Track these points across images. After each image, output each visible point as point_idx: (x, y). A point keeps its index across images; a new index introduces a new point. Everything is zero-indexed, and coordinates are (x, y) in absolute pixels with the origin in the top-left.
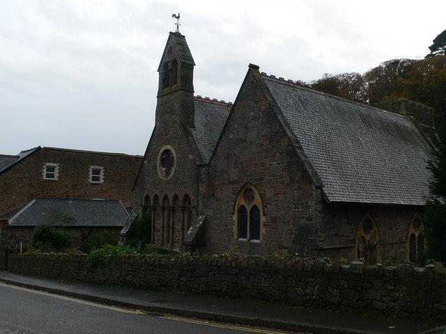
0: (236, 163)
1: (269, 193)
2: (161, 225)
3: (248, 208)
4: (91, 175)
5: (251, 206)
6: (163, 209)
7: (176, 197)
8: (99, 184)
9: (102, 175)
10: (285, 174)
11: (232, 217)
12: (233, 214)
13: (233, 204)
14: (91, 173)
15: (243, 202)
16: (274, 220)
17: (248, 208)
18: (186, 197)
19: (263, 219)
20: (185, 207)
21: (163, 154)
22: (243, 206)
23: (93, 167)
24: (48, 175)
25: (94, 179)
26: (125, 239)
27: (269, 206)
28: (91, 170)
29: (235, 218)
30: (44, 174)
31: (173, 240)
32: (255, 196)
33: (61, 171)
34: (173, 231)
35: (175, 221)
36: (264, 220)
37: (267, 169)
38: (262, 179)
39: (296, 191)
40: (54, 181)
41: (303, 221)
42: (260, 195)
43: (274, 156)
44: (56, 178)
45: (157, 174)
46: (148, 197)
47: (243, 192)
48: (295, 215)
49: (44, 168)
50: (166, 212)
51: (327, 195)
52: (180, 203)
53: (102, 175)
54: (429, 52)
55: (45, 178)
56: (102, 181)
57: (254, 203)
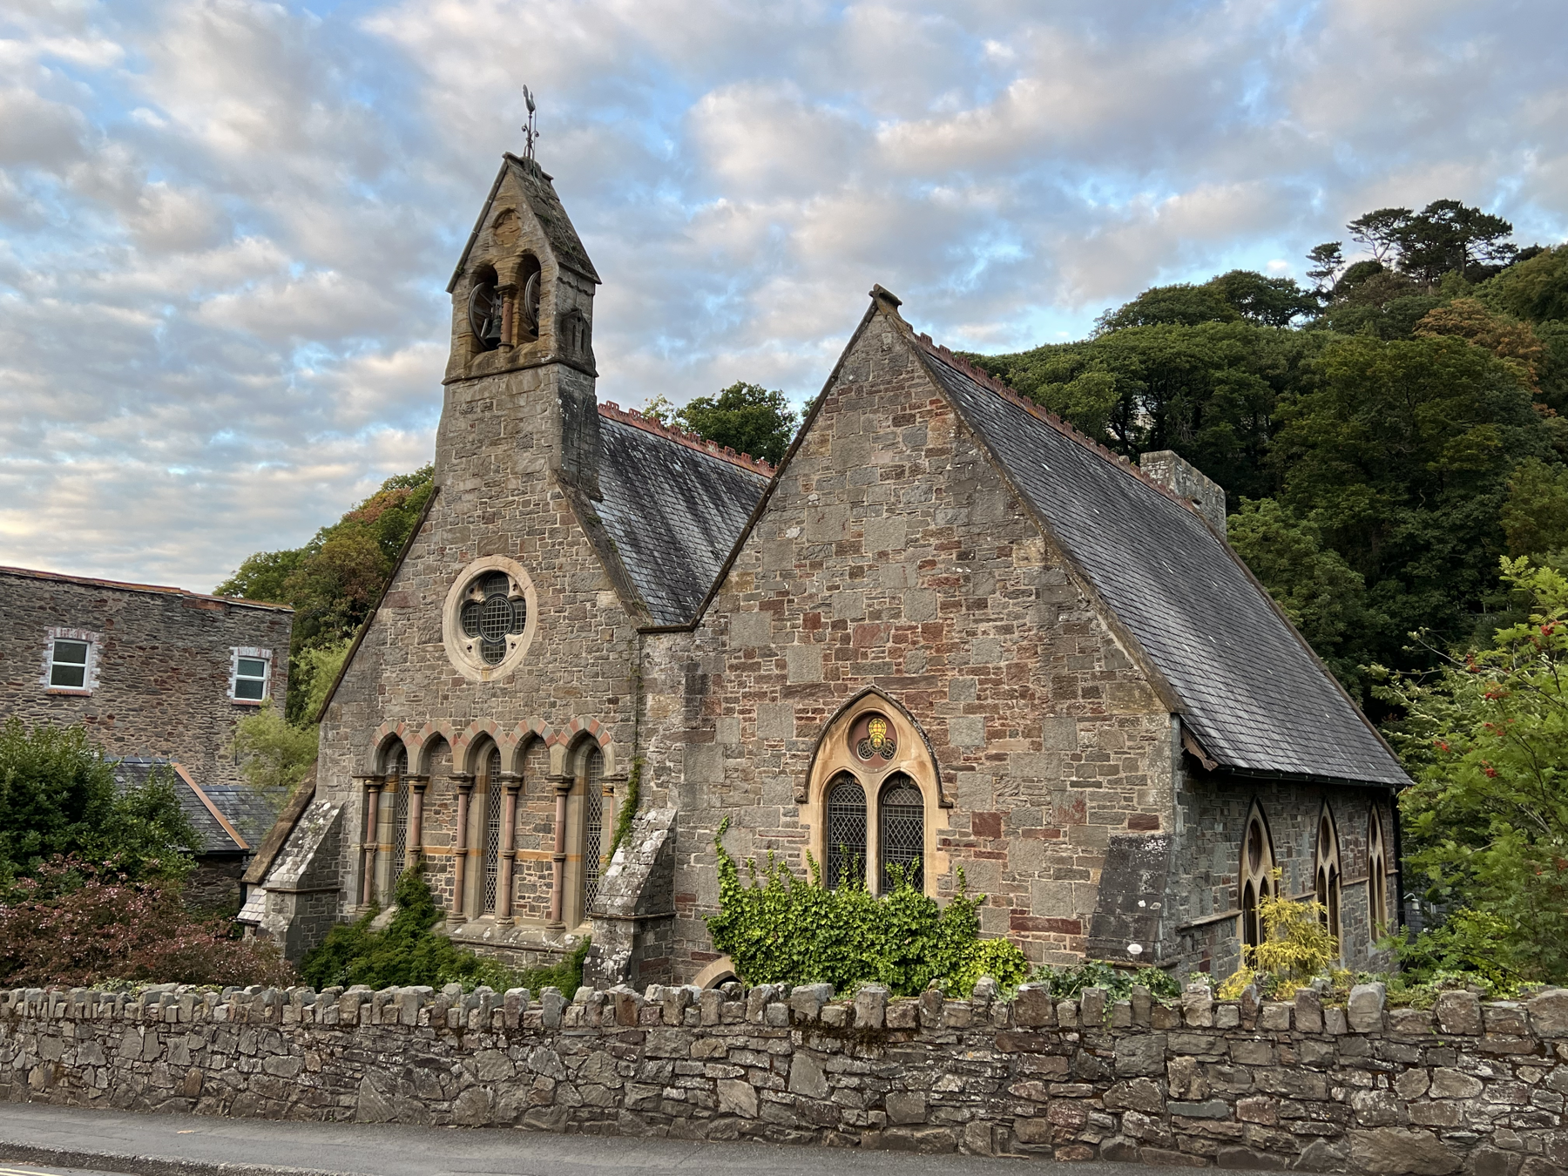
0: (813, 622)
1: (964, 732)
2: (457, 847)
3: (870, 783)
4: (50, 661)
5: (881, 778)
6: (468, 786)
7: (436, 743)
8: (257, 707)
9: (91, 664)
10: (1032, 663)
11: (795, 813)
12: (803, 800)
13: (801, 765)
14: (49, 654)
15: (838, 756)
16: (988, 825)
17: (870, 783)
18: (584, 743)
19: (935, 823)
20: (572, 781)
21: (470, 588)
22: (846, 775)
25: (60, 676)
26: (291, 903)
28: (235, 659)
31: (510, 899)
34: (513, 870)
35: (524, 829)
36: (944, 825)
37: (953, 647)
46: (392, 744)
47: (845, 724)
48: (1080, 805)
49: (45, 647)
50: (478, 800)
52: (456, 761)
53: (91, 664)
54: (450, 295)
56: (89, 684)
57: (891, 767)
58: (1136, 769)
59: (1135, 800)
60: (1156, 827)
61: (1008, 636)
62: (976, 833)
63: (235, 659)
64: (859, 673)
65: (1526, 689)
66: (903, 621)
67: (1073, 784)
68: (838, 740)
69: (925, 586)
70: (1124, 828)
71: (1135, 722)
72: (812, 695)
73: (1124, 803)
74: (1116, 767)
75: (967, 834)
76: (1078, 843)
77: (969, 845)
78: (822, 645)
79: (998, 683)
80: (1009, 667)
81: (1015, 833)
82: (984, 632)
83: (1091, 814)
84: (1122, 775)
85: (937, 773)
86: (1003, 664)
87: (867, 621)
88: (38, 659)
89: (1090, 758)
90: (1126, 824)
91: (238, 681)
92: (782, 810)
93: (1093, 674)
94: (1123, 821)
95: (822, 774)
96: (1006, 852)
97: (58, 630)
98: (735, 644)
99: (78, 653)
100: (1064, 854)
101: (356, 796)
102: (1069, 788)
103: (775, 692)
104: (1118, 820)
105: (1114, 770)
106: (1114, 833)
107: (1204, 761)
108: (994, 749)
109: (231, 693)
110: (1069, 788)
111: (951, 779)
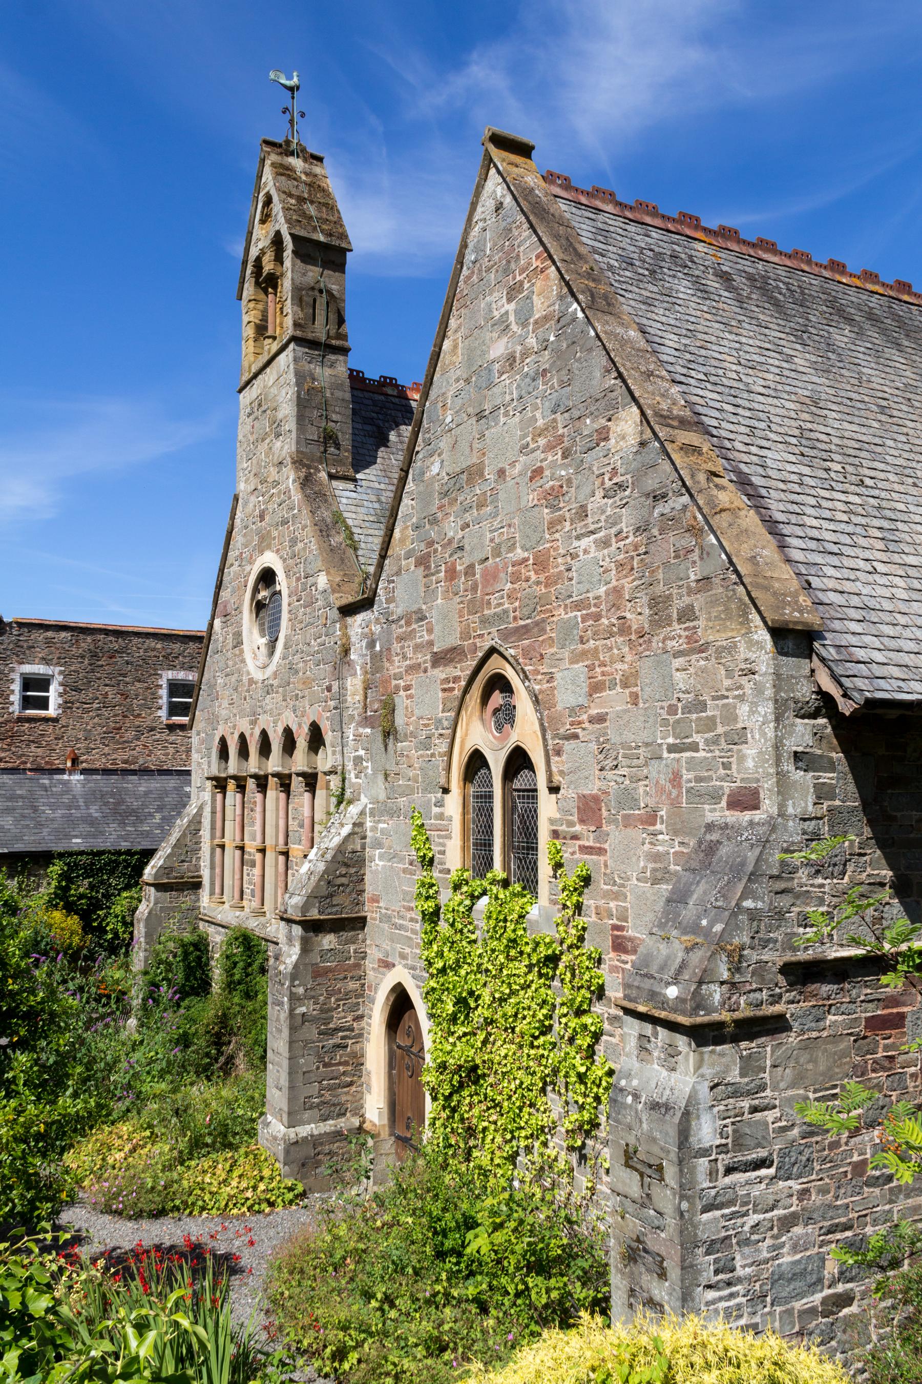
10: (628, 584)
11: (440, 804)
13: (444, 748)
14: (164, 692)
21: (256, 590)
23: (170, 674)
24: (27, 702)
27: (568, 746)
29: (453, 805)
30: (15, 698)
32: (519, 712)
33: (69, 687)
38: (540, 626)
39: (679, 662)
40: (46, 720)
41: (717, 813)
42: (536, 701)
43: (582, 513)
44: (52, 712)
45: (243, 661)
48: (676, 779)
49: (13, 681)
51: (346, 515)
53: (54, 694)
55: (16, 708)
58: (735, 719)
59: (734, 766)
60: (756, 807)
61: (606, 551)
62: (582, 821)
63: (163, 682)
64: (485, 628)
65: (428, 555)
66: (519, 553)
67: (672, 749)
68: (471, 713)
69: (535, 502)
70: (722, 809)
71: (731, 649)
72: (452, 660)
73: (722, 772)
74: (712, 719)
75: (571, 824)
76: (676, 833)
77: (575, 837)
78: (457, 599)
79: (597, 617)
80: (607, 594)
81: (615, 821)
82: (586, 552)
83: (687, 792)
84: (720, 730)
85: (545, 746)
86: (602, 590)
87: (491, 561)
88: (156, 697)
89: (688, 709)
90: (724, 804)
91: (48, 691)
92: (433, 800)
93: (689, 587)
94: (720, 798)
95: (461, 753)
96: (606, 846)
97: (170, 672)
98: (399, 611)
99: (43, 683)
100: (660, 848)
101: (207, 796)
102: (665, 755)
103: (425, 662)
104: (715, 797)
105: (710, 724)
106: (710, 817)
107: (840, 700)
108: (596, 708)
109: (163, 713)
110: (665, 755)
111: (558, 753)
